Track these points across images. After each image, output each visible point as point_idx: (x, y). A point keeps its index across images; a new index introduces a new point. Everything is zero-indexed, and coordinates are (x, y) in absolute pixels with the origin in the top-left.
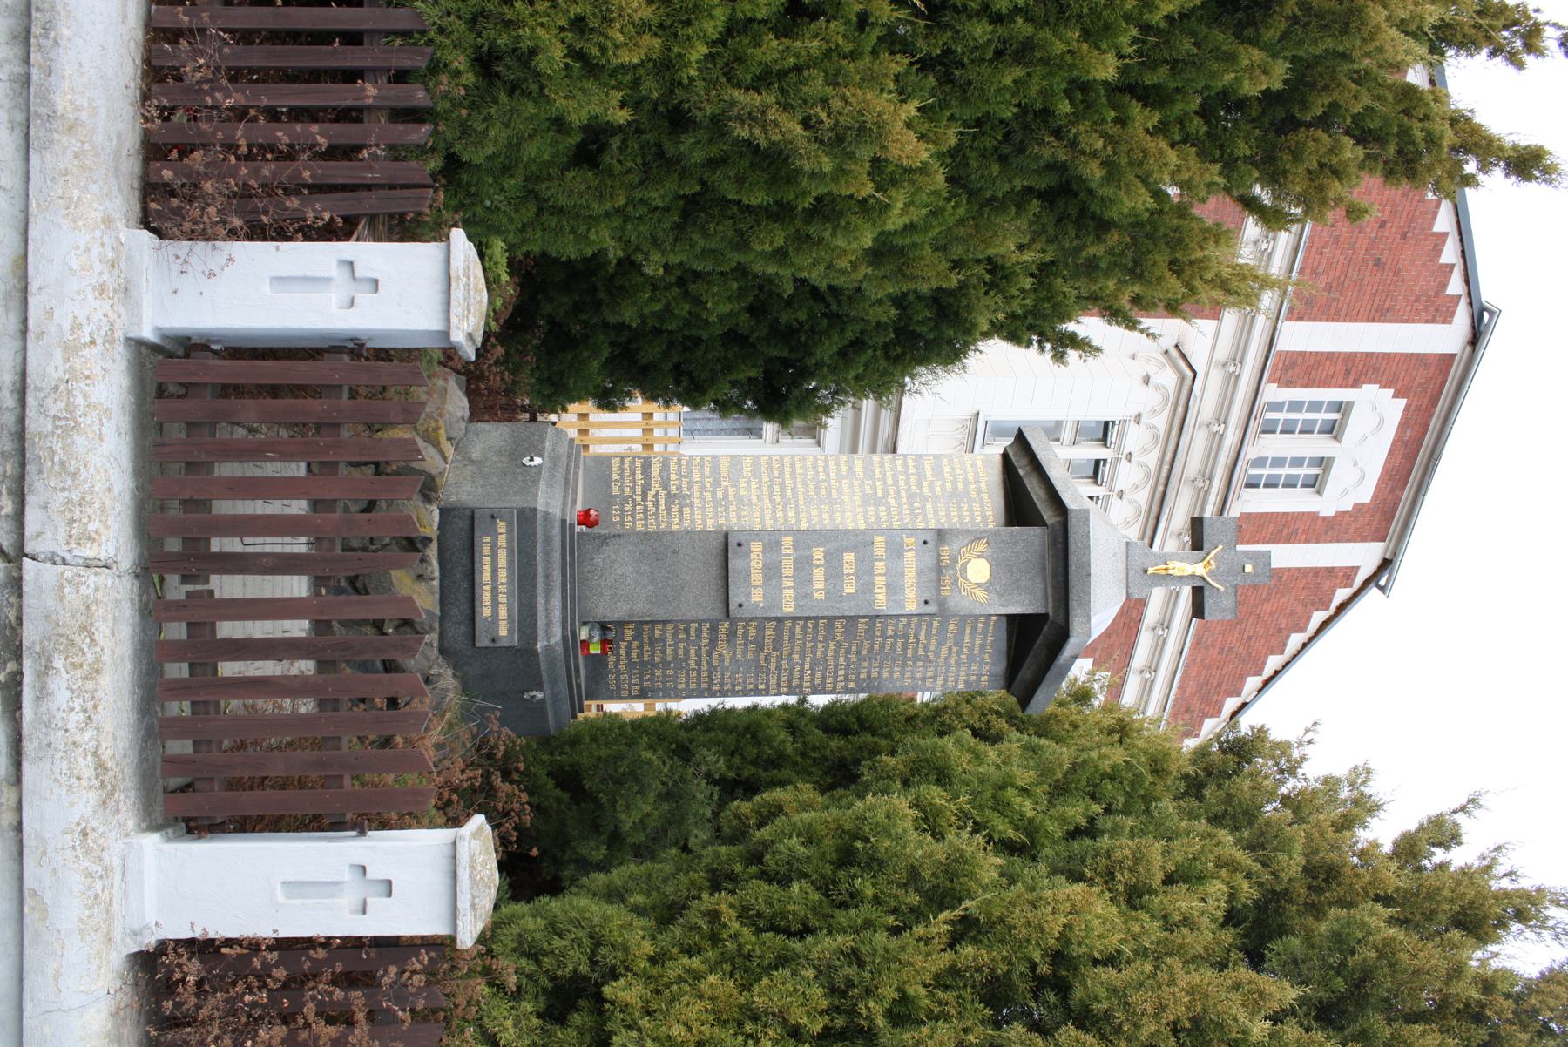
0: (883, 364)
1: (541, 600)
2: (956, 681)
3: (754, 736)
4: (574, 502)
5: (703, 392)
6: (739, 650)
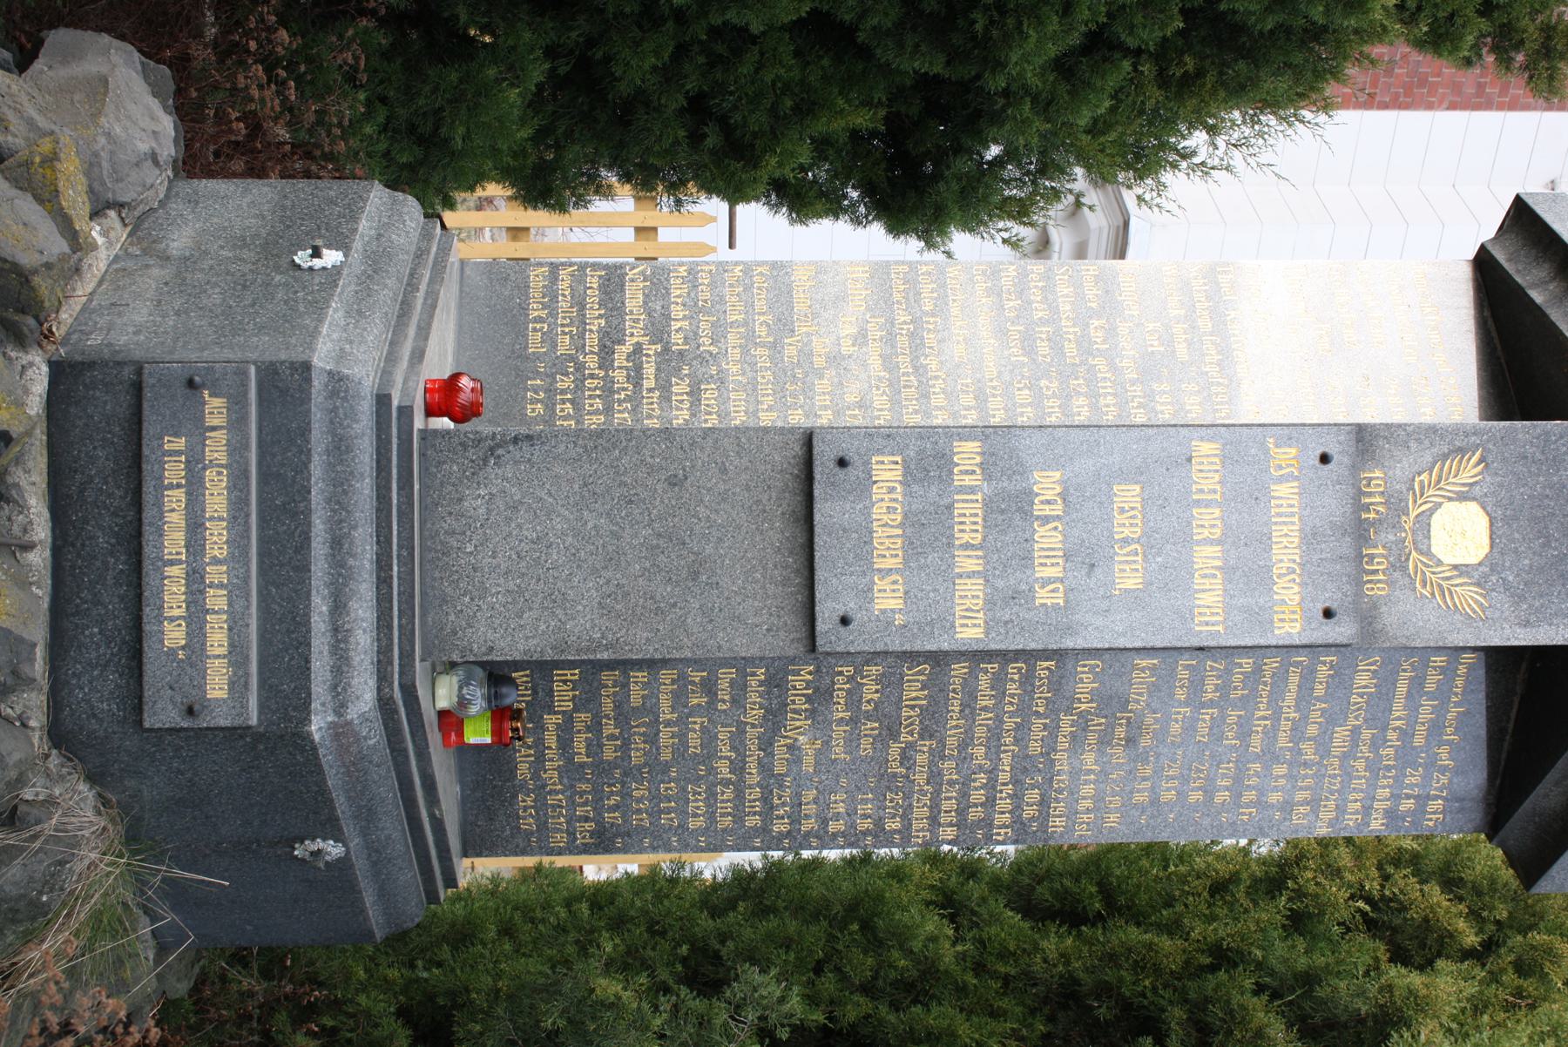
0: (1154, 95)
1: (320, 606)
2: (1367, 810)
3: (866, 926)
4: (418, 355)
5: (754, 162)
6: (839, 732)
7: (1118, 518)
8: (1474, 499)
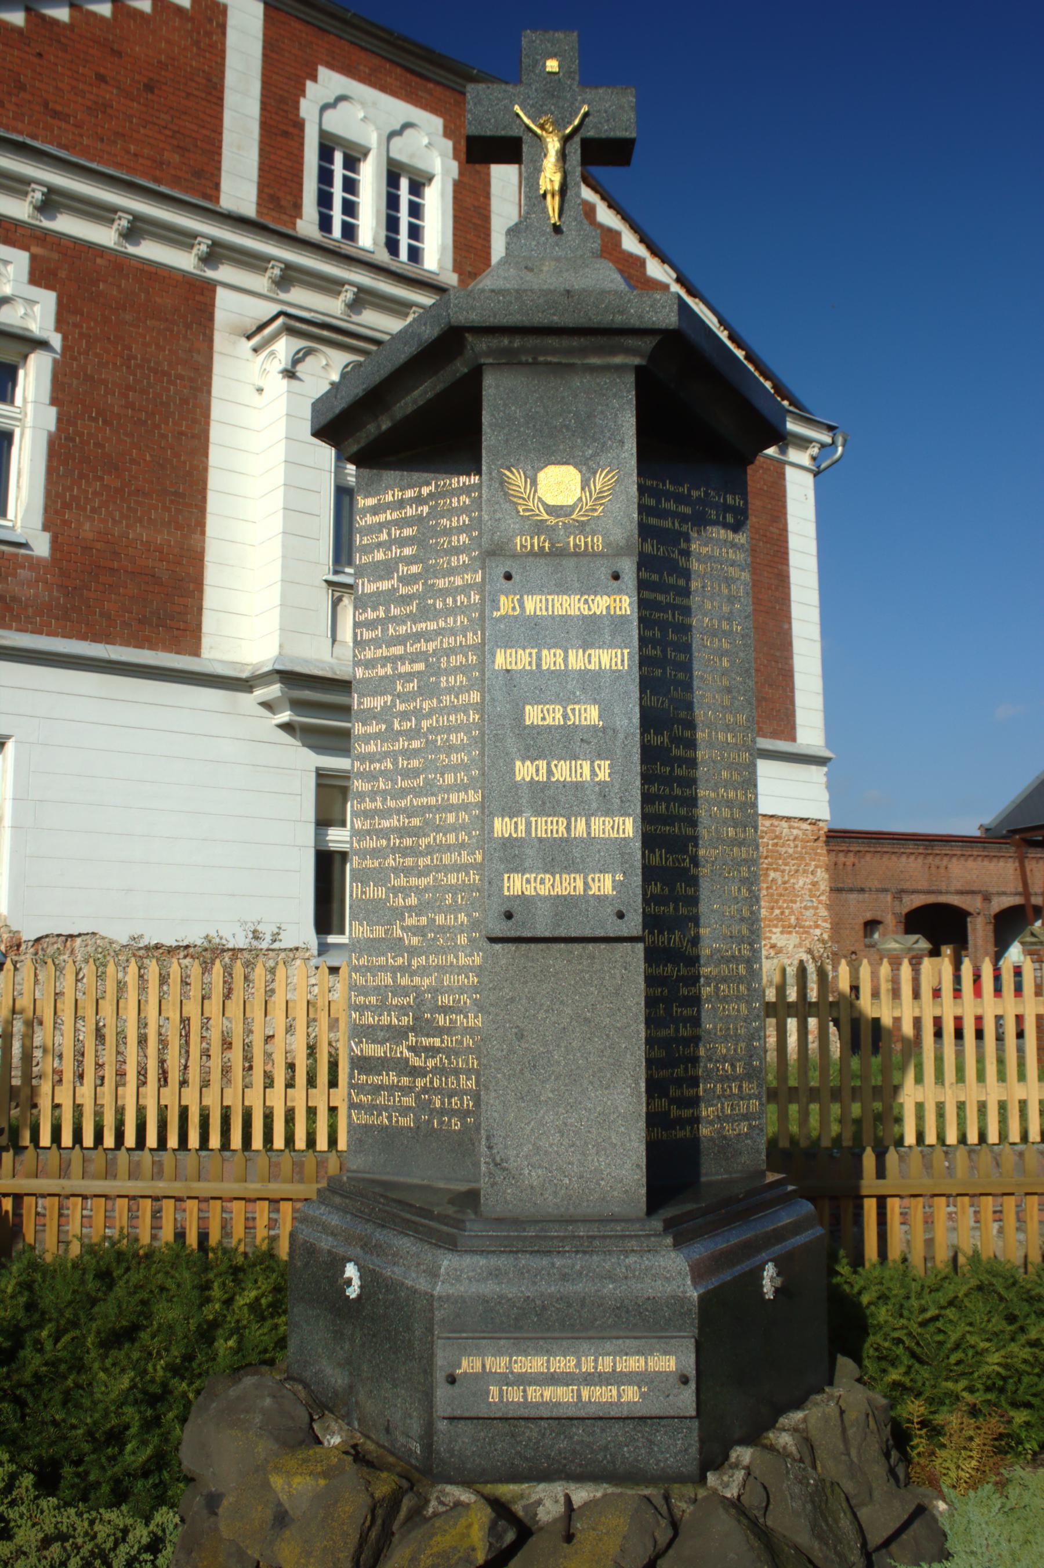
7: (549, 721)
8: (536, 475)
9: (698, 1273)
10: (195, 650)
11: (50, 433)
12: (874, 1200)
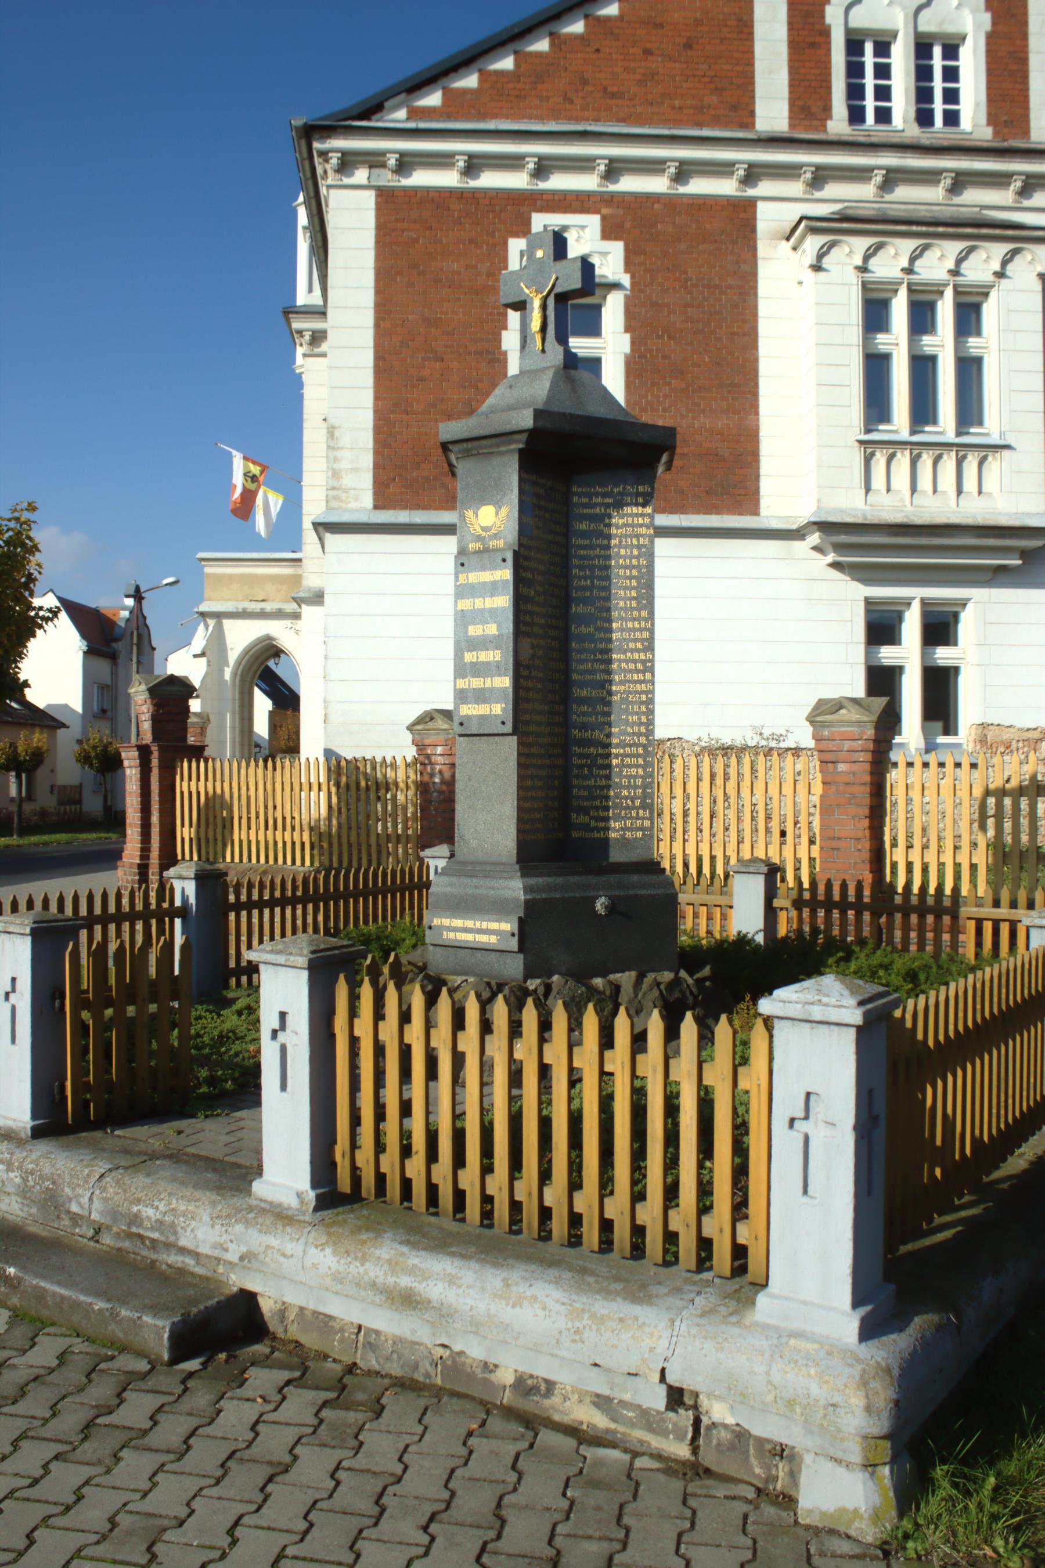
9: (527, 889)
10: (755, 511)
11: (626, 356)
12: (973, 922)
